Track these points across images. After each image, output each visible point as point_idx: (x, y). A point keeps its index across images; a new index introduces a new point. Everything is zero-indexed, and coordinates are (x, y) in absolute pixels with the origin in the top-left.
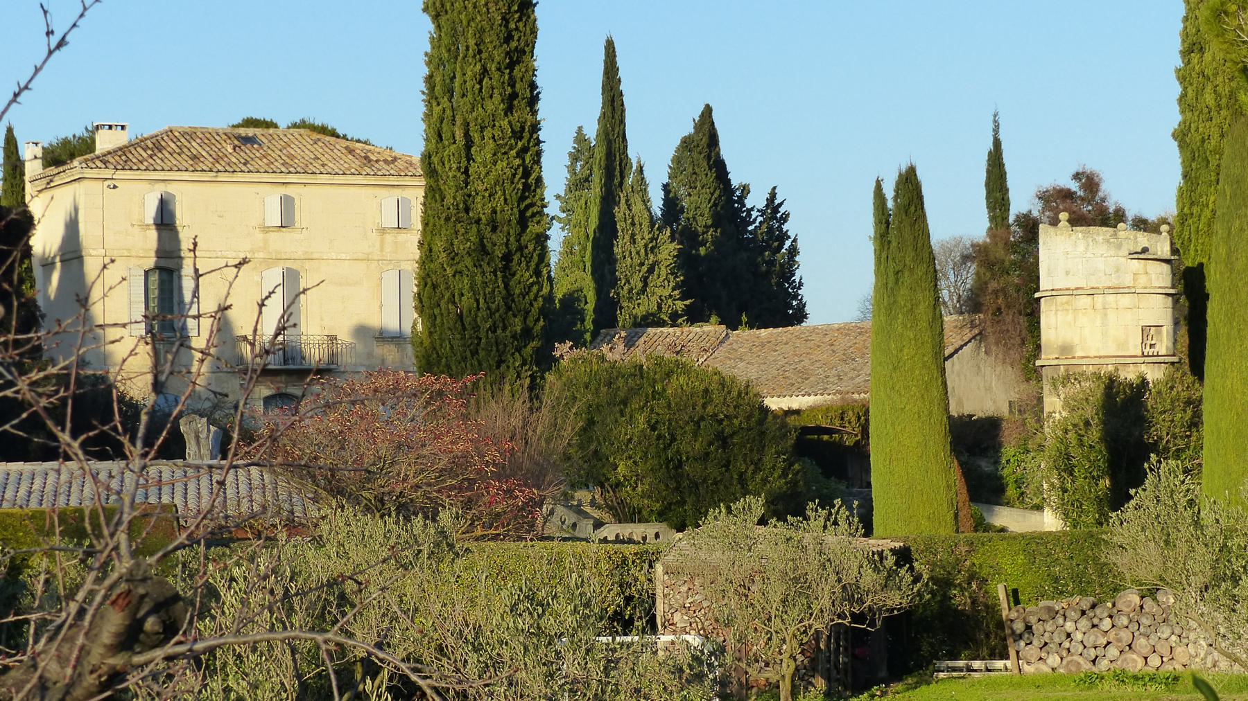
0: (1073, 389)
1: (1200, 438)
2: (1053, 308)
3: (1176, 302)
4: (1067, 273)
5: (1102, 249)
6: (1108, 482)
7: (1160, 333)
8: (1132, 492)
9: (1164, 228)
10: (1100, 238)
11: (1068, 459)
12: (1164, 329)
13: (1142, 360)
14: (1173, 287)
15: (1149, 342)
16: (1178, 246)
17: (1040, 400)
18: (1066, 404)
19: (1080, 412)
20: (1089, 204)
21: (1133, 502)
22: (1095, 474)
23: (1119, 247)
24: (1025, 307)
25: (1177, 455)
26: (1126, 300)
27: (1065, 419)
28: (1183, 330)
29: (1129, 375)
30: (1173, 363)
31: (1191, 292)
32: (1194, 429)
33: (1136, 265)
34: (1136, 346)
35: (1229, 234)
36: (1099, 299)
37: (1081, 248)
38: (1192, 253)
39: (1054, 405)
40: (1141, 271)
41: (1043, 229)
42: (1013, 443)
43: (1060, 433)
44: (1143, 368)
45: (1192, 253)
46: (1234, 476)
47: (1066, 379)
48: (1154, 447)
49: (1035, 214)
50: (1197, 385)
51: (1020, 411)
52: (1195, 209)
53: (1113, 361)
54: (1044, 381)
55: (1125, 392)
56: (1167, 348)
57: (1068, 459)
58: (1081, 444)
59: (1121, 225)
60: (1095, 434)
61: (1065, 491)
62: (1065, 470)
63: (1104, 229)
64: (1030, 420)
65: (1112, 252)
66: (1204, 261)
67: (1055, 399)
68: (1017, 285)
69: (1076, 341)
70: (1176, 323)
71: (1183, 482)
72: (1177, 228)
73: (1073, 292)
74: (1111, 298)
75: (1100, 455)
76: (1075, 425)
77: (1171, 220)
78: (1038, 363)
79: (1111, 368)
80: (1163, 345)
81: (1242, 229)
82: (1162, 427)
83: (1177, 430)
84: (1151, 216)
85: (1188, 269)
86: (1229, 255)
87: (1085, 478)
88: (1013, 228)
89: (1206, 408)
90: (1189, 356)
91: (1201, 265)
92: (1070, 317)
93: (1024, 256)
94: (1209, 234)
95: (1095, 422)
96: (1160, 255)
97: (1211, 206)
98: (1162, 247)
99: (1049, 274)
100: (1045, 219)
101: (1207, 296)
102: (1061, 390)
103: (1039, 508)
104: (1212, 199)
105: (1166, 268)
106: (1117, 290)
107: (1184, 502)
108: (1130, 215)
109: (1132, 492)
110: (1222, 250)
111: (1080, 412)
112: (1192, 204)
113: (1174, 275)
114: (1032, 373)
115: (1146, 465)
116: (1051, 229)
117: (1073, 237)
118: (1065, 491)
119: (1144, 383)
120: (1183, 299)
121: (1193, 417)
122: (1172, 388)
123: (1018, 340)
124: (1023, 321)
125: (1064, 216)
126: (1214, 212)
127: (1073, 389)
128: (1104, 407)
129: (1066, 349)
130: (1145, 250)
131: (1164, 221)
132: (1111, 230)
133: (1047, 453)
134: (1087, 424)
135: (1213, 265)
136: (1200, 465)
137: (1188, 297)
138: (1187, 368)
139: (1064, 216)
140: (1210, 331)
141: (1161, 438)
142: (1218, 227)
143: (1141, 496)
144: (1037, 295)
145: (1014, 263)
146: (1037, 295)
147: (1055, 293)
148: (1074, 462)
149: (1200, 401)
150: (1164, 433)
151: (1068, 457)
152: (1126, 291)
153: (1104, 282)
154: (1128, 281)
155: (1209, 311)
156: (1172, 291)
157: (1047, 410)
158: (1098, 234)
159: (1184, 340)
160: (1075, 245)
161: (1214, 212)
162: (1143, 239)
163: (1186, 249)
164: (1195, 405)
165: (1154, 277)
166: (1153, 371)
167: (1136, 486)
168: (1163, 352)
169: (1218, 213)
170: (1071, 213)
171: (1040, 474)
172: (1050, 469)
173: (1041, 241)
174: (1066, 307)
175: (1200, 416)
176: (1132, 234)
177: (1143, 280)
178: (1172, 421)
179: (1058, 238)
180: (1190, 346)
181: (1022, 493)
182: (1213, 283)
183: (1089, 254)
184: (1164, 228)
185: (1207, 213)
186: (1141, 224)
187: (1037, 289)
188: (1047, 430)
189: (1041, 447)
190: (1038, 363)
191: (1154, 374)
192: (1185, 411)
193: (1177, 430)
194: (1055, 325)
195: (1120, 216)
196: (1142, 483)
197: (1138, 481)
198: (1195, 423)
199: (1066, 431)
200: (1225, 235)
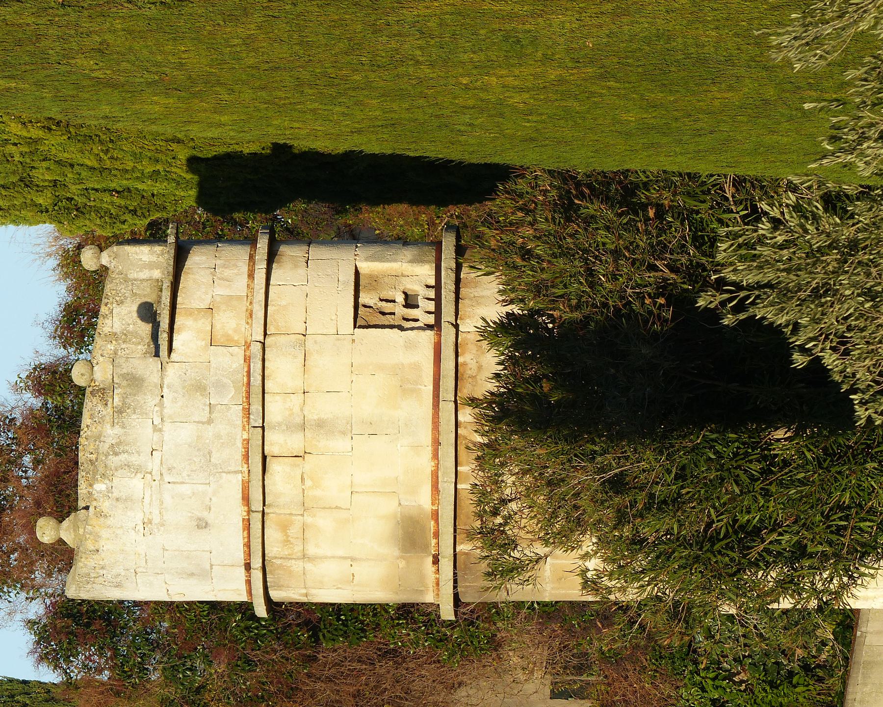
0: (525, 527)
1: (666, 180)
2: (297, 566)
3: (294, 236)
4: (202, 525)
5: (140, 429)
6: (780, 434)
7: (376, 281)
8: (799, 360)
9: (89, 259)
10: (111, 433)
11: (714, 539)
12: (366, 267)
13: (448, 333)
14: (252, 241)
15: (400, 310)
16: (141, 224)
17: (551, 612)
18: (564, 539)
19: (584, 502)
20: (15, 462)
21: (830, 360)
22: (755, 467)
23: (135, 382)
24: (295, 645)
25: (706, 242)
26: (283, 369)
27: (603, 542)
28: (373, 217)
29: (485, 367)
30: (460, 251)
31: (266, 194)
32: (642, 196)
33: (188, 337)
34: (410, 346)
35: (114, 86)
36: (276, 442)
37: (135, 485)
38: (159, 187)
39: (561, 573)
40: (204, 324)
41: (80, 588)
42: (667, 690)
43: (641, 561)
44: (469, 326)
45: (159, 187)
46: (770, 92)
47: (496, 539)
48: (682, 302)
49: (36, 609)
50: (522, 185)
51: (580, 669)
52: (42, 174)
53: (447, 408)
54: (500, 596)
55: (536, 379)
56: (418, 260)
57: (714, 539)
58: (674, 503)
59: (78, 375)
60: (647, 464)
61: (800, 551)
62: (745, 550)
63: (86, 420)
64: (606, 639)
65: (151, 401)
66: (183, 154)
67: (547, 569)
68: (232, 667)
69: (389, 507)
70: (352, 236)
71: (777, 223)
72: (93, 225)
73: (257, 511)
74: (276, 409)
75: (708, 446)
76: (621, 518)
77: (69, 243)
78: (447, 613)
79: (467, 415)
80: (411, 272)
81: (101, 51)
82: (630, 281)
83: (642, 242)
84: (52, 294)
85: (203, 199)
86: (169, 88)
87: (767, 494)
88: (76, 674)
89: (582, 161)
90: (442, 202)
91: (193, 163)
92: (323, 522)
93: (155, 646)
94: (108, 138)
95: (613, 463)
96: (232, 469)
97: (35, 133)
98: (140, 266)
99: (204, 574)
100: (54, 583)
101: (281, 150)
102: (527, 549)
103: (848, 624)
104: (15, 128)
105: (199, 259)
106: (255, 391)
107: (830, 221)
108: (50, 351)
109: (799, 360)
110: (156, 104)
111: (584, 502)
112: (27, 183)
113: (218, 239)
114: (477, 632)
115: (728, 320)
116: (82, 565)
117: (105, 505)
118: (800, 551)
119: (507, 330)
120: (287, 216)
121: (607, 200)
122: (527, 254)
123: (384, 667)
124: (331, 651)
125: (47, 531)
126: (51, 125)
127: (525, 527)
128: (573, 438)
129: (412, 536)
130: (148, 313)
131: (70, 262)
132: (90, 405)
133: (697, 597)
134: (618, 484)
135: (195, 131)
136: (739, 182)
137: (282, 203)
138: (474, 211)
139: (47, 531)
140: (373, 145)
141: (663, 288)
142: (94, 113)
143: (810, 335)
144: (261, 611)
145: (171, 674)
146: (261, 611)
147: (259, 563)
148: (721, 524)
149: (565, 177)
150: (650, 277)
151: (708, 539)
152: (257, 366)
153: (230, 427)
154: (230, 361)
155: (322, 145)
156: (263, 244)
157: (573, 592)
158: (98, 438)
159: (398, 215)
160: (125, 501)
161: (51, 125)
162: (119, 317)
163: (150, 201)
164: (574, 192)
165: (220, 291)
166: (477, 301)
167: (785, 350)
168: (426, 272)
169: (54, 112)
170: (39, 509)
171: (753, 619)
172: (740, 590)
173: (114, 595)
174: (294, 531)
175: (606, 179)
176: (101, 347)
177: (230, 322)
178: (616, 254)
179: (106, 545)
180: (413, 202)
181: (806, 668)
182: (241, 131)
183: (154, 464)
184: (89, 259)
185: (53, 142)
186: (78, 322)
187: (245, 608)
188: (632, 595)
189: (680, 613)
190: (447, 613)
191: (487, 300)
192: (589, 220)
193: (642, 242)
194: (346, 560)
195: (52, 380)
196: (775, 331)
197: (773, 342)
198: (623, 192)
199: (638, 543)
200: (116, 96)
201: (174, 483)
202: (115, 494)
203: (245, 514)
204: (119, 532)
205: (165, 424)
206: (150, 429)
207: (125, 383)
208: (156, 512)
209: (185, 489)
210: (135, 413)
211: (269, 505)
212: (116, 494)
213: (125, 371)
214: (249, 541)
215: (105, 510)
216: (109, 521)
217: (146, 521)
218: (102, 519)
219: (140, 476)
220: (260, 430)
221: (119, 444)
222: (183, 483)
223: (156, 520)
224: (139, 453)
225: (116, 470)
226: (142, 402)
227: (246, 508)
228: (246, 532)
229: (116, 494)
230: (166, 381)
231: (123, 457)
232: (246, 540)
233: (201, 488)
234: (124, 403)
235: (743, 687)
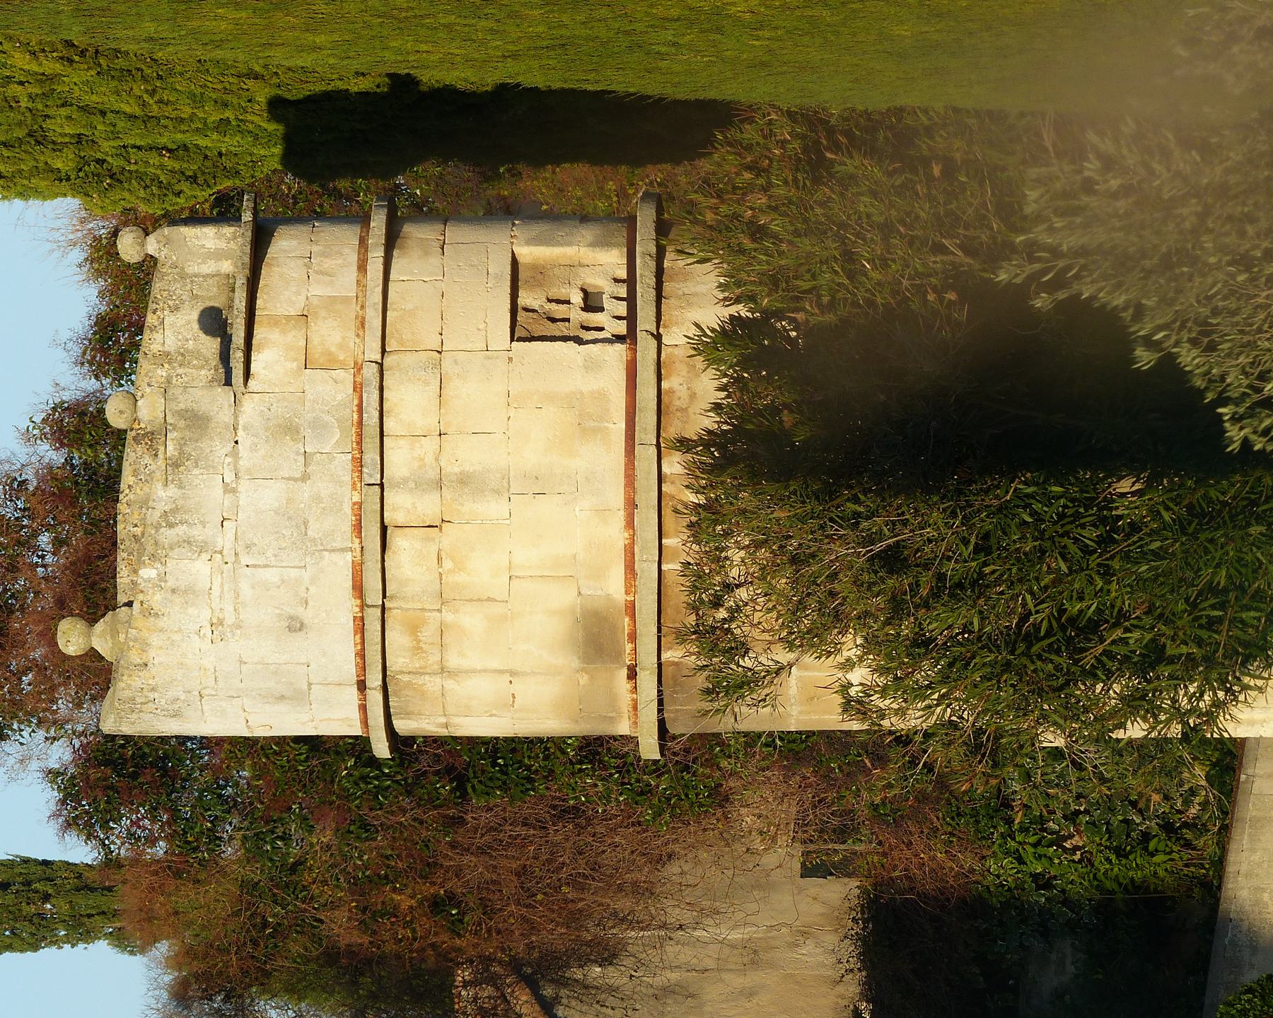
201: (255, 566)
203: (358, 609)
204: (177, 637)
205: (241, 481)
206: (219, 490)
207: (182, 423)
209: (271, 575)
210: (197, 466)
212: (171, 583)
213: (182, 406)
214: (363, 649)
216: (162, 623)
217: (215, 621)
218: (152, 619)
219: (205, 556)
221: (175, 510)
222: (266, 566)
223: (230, 619)
224: (203, 524)
225: (172, 548)
228: (358, 636)
229: (171, 583)
231: (181, 530)
232: (359, 647)
233: (294, 573)
234: (181, 453)
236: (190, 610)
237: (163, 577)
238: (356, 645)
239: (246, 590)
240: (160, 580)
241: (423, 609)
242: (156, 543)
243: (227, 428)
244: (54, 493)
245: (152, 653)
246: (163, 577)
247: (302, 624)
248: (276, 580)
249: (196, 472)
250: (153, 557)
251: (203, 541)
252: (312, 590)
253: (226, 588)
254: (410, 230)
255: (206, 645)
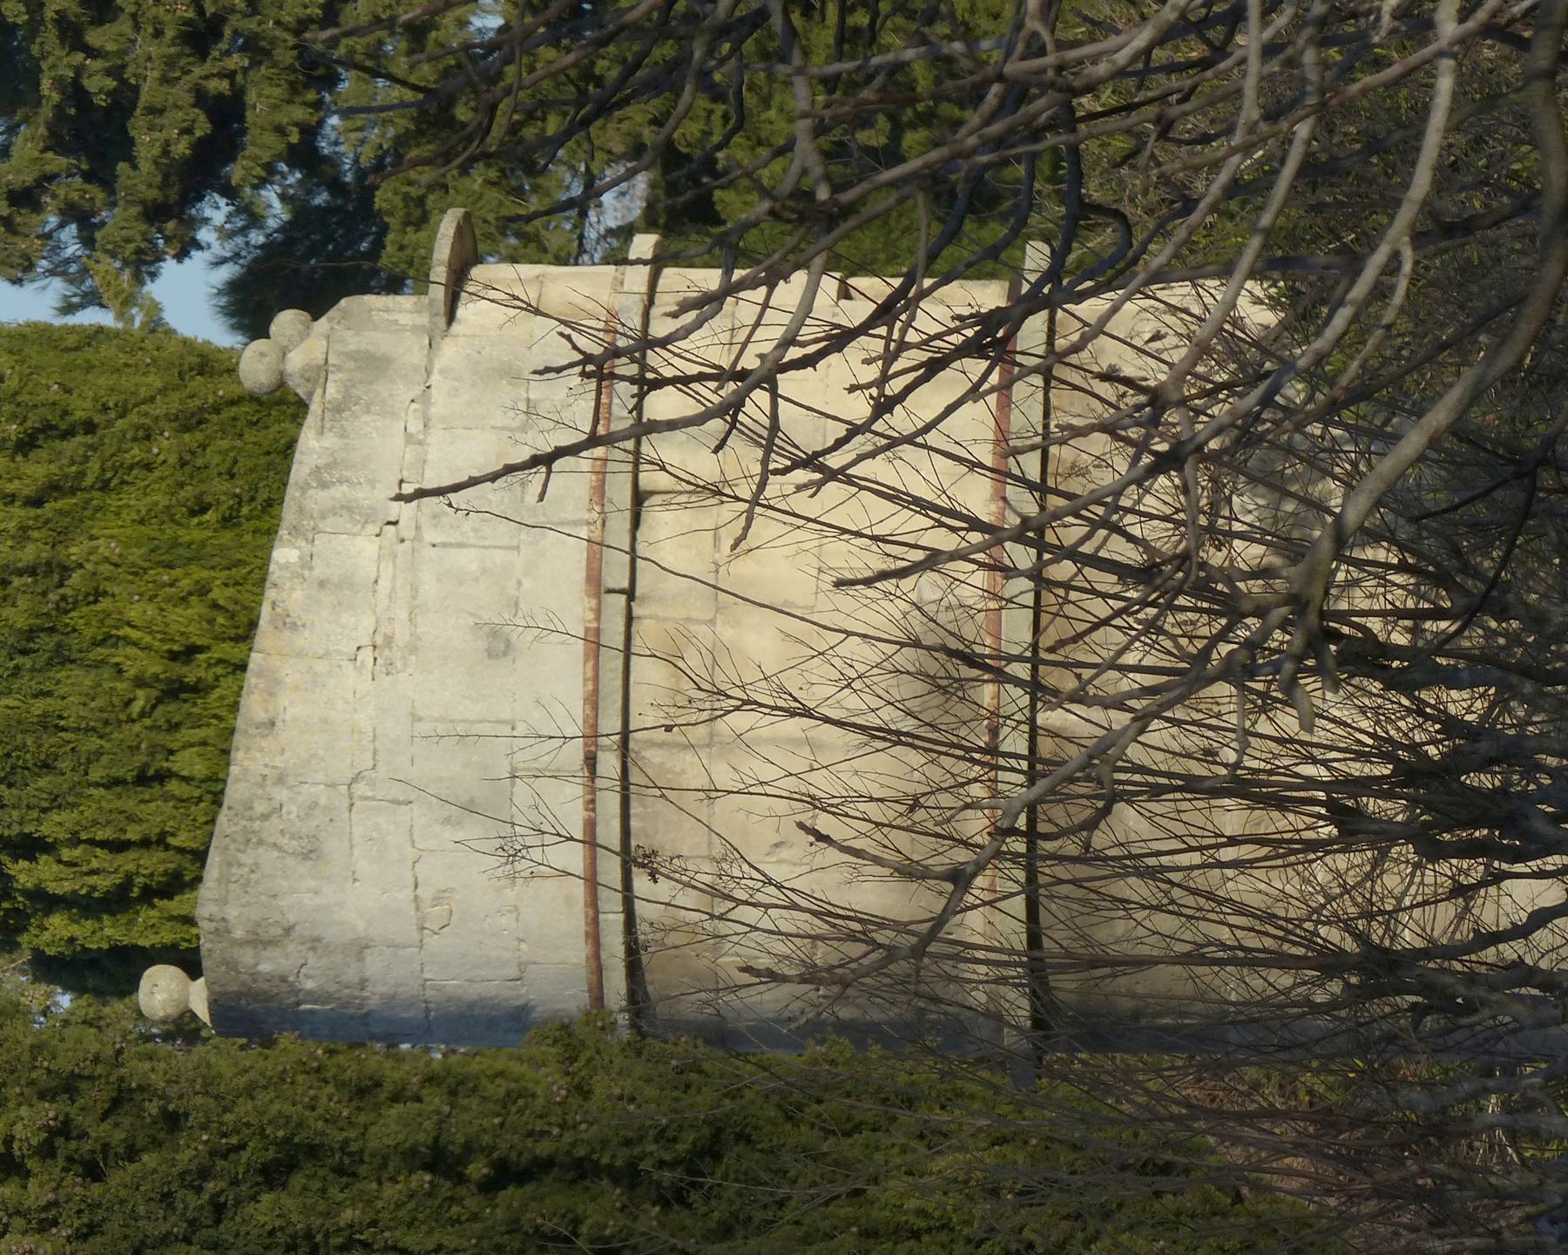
160: (339, 588)
179: (292, 707)
201: (445, 545)
202: (316, 572)
203: (591, 615)
204: (321, 667)
205: (432, 431)
206: (399, 440)
207: (351, 365)
208: (403, 615)
209: (467, 560)
210: (368, 412)
211: (644, 598)
212: (319, 571)
213: (353, 347)
214: (596, 691)
215: (295, 611)
216: (302, 640)
217: (379, 640)
218: (287, 633)
219: (372, 529)
220: (623, 598)
221: (332, 465)
222: (461, 545)
223: (402, 636)
224: (372, 483)
225: (323, 517)
226: (386, 394)
227: (594, 602)
228: (590, 664)
229: (319, 571)
230: (437, 366)
231: (339, 491)
232: (590, 687)
233: (499, 556)
234: (347, 396)
235: (1520, 427)
236: (346, 618)
237: (307, 562)
238: (585, 680)
239: (429, 588)
240: (302, 567)
241: (689, 619)
242: (301, 510)
243: (415, 369)
244: (173, 835)
245: (284, 699)
246: (307, 562)
247: (508, 644)
248: (473, 567)
249: (366, 418)
250: (296, 530)
251: (370, 507)
252: (527, 583)
253: (399, 582)
254: (584, 999)
255: (366, 685)
